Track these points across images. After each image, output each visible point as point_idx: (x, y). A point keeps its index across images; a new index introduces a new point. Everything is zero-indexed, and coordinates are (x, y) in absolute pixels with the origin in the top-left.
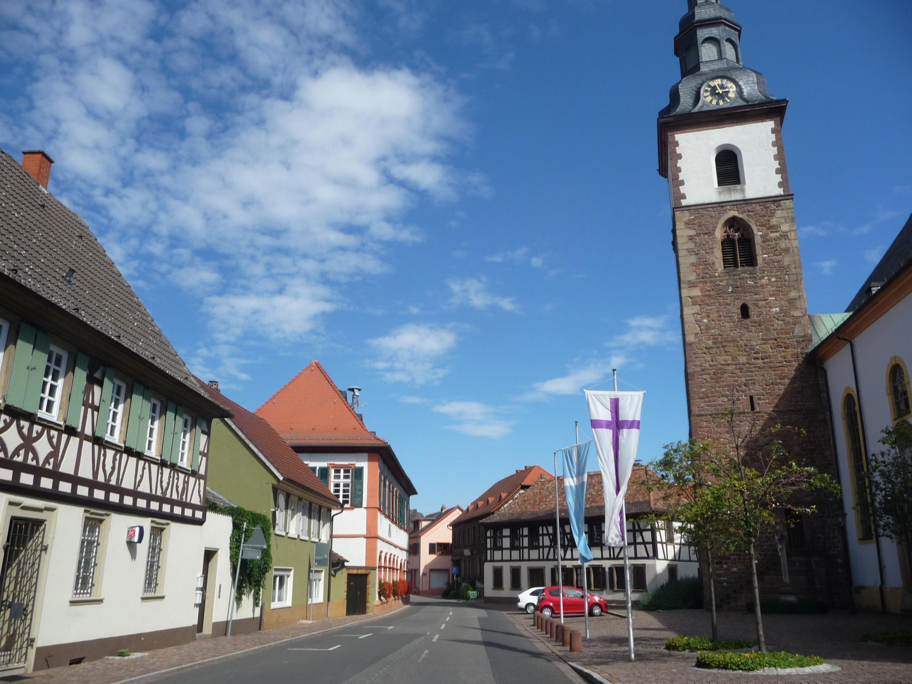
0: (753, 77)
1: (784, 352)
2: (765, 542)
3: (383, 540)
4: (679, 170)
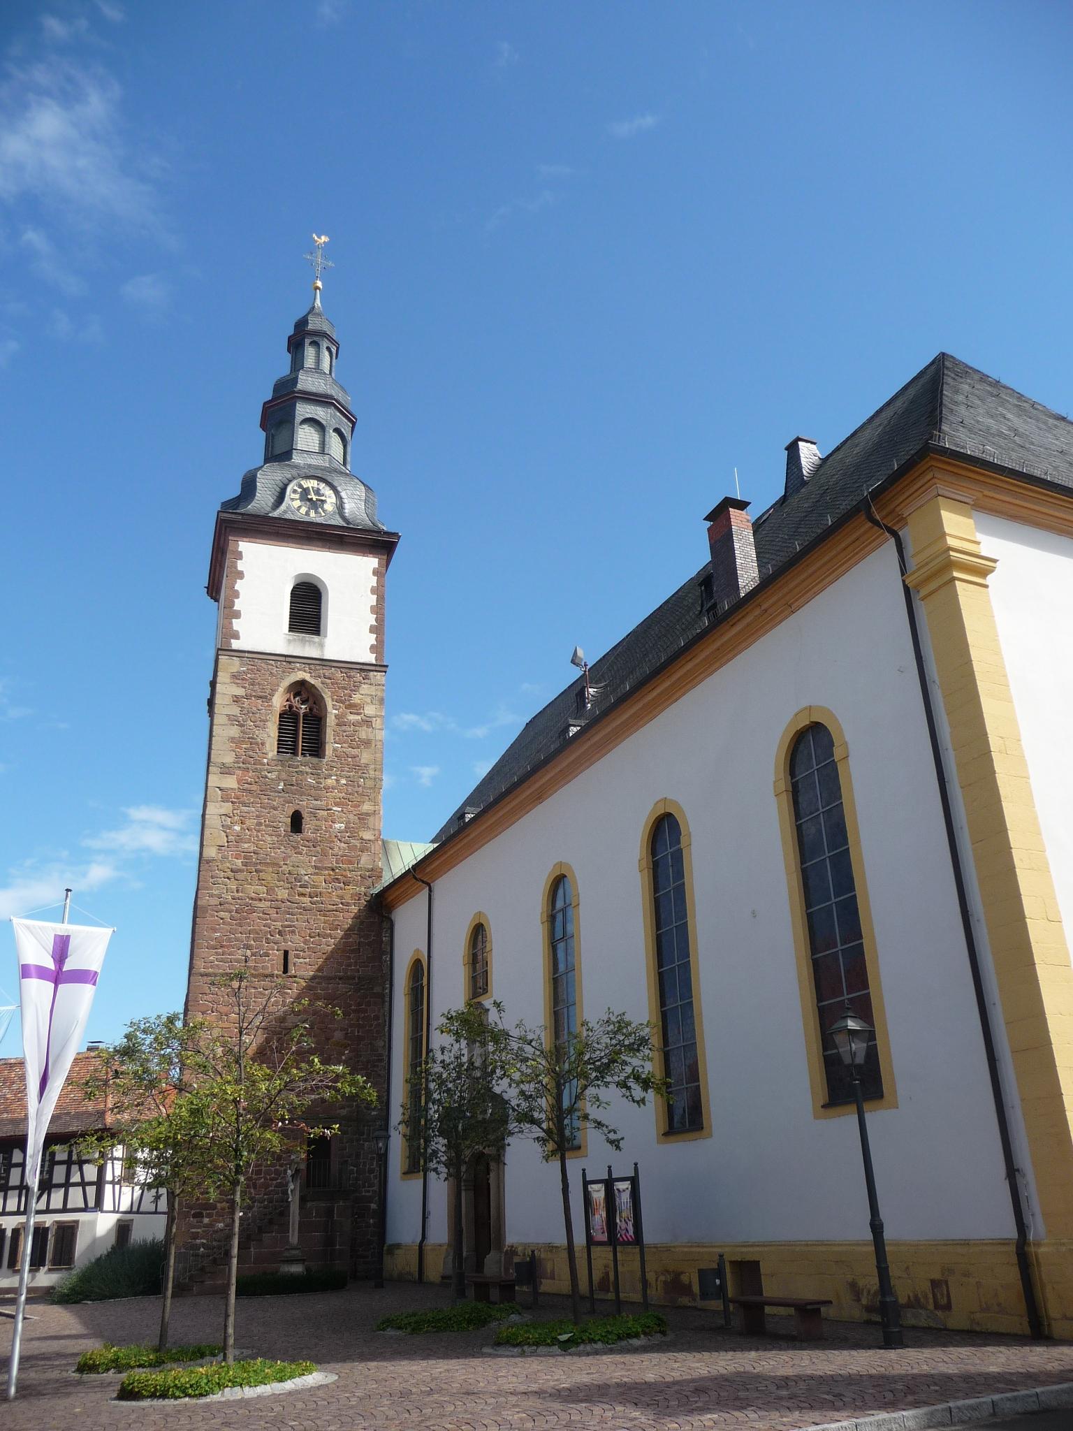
0: (361, 491)
1: (341, 889)
2: (272, 1179)
4: (236, 594)
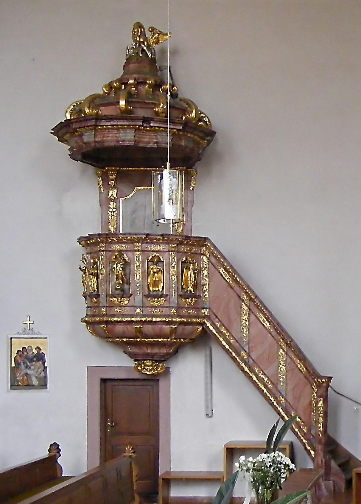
3: (106, 293)
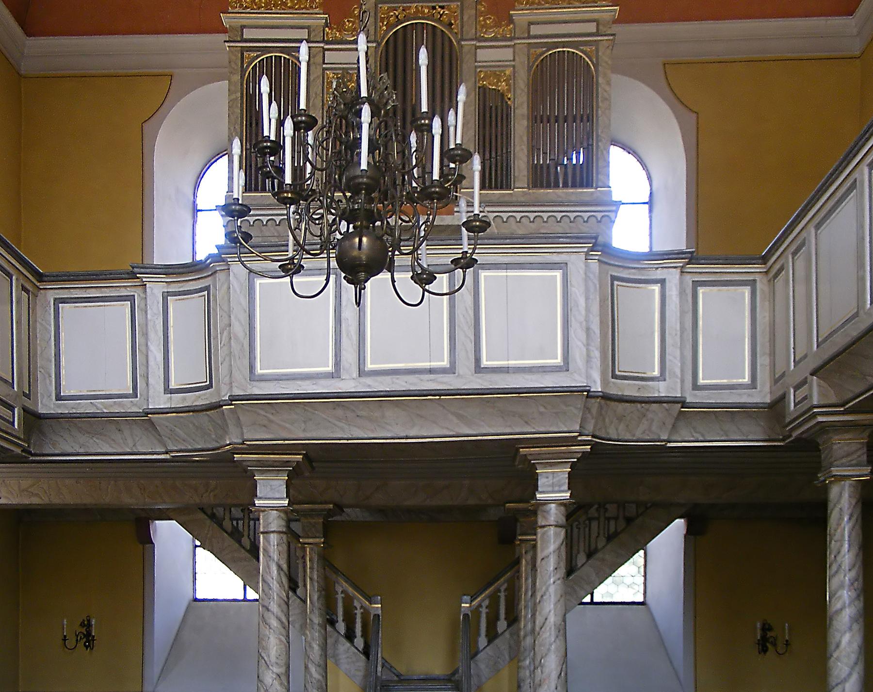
3: (606, 545)
